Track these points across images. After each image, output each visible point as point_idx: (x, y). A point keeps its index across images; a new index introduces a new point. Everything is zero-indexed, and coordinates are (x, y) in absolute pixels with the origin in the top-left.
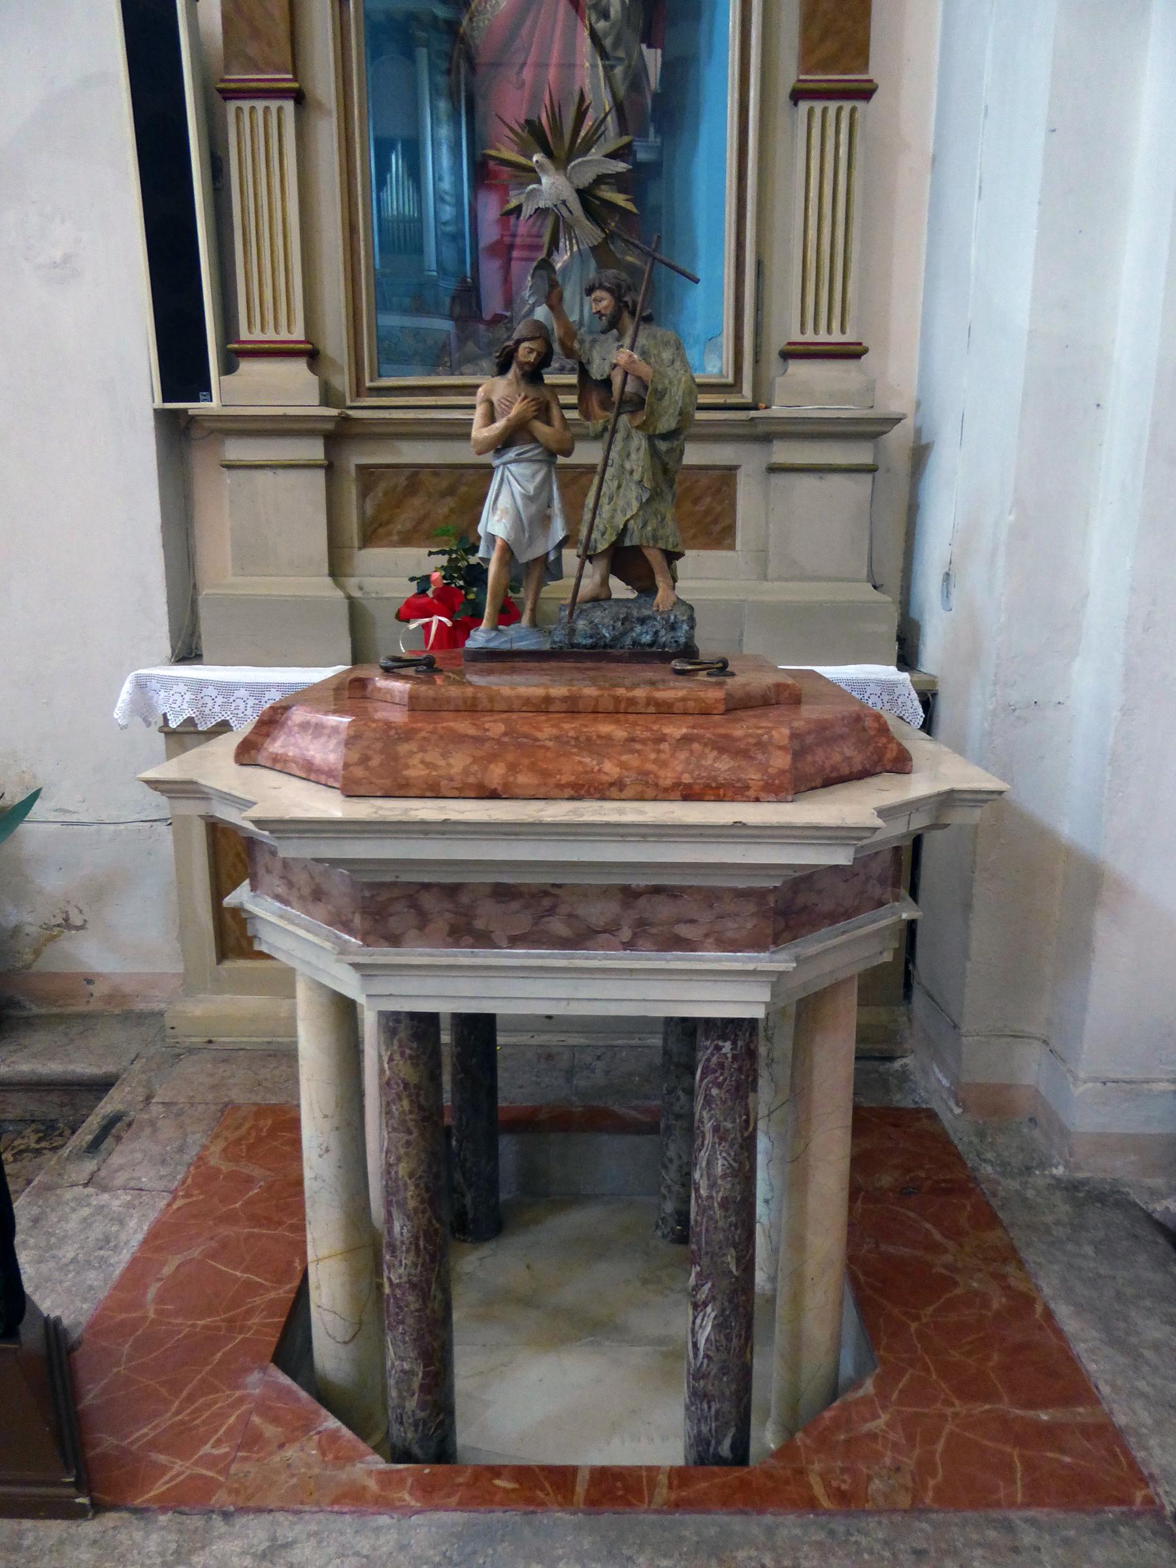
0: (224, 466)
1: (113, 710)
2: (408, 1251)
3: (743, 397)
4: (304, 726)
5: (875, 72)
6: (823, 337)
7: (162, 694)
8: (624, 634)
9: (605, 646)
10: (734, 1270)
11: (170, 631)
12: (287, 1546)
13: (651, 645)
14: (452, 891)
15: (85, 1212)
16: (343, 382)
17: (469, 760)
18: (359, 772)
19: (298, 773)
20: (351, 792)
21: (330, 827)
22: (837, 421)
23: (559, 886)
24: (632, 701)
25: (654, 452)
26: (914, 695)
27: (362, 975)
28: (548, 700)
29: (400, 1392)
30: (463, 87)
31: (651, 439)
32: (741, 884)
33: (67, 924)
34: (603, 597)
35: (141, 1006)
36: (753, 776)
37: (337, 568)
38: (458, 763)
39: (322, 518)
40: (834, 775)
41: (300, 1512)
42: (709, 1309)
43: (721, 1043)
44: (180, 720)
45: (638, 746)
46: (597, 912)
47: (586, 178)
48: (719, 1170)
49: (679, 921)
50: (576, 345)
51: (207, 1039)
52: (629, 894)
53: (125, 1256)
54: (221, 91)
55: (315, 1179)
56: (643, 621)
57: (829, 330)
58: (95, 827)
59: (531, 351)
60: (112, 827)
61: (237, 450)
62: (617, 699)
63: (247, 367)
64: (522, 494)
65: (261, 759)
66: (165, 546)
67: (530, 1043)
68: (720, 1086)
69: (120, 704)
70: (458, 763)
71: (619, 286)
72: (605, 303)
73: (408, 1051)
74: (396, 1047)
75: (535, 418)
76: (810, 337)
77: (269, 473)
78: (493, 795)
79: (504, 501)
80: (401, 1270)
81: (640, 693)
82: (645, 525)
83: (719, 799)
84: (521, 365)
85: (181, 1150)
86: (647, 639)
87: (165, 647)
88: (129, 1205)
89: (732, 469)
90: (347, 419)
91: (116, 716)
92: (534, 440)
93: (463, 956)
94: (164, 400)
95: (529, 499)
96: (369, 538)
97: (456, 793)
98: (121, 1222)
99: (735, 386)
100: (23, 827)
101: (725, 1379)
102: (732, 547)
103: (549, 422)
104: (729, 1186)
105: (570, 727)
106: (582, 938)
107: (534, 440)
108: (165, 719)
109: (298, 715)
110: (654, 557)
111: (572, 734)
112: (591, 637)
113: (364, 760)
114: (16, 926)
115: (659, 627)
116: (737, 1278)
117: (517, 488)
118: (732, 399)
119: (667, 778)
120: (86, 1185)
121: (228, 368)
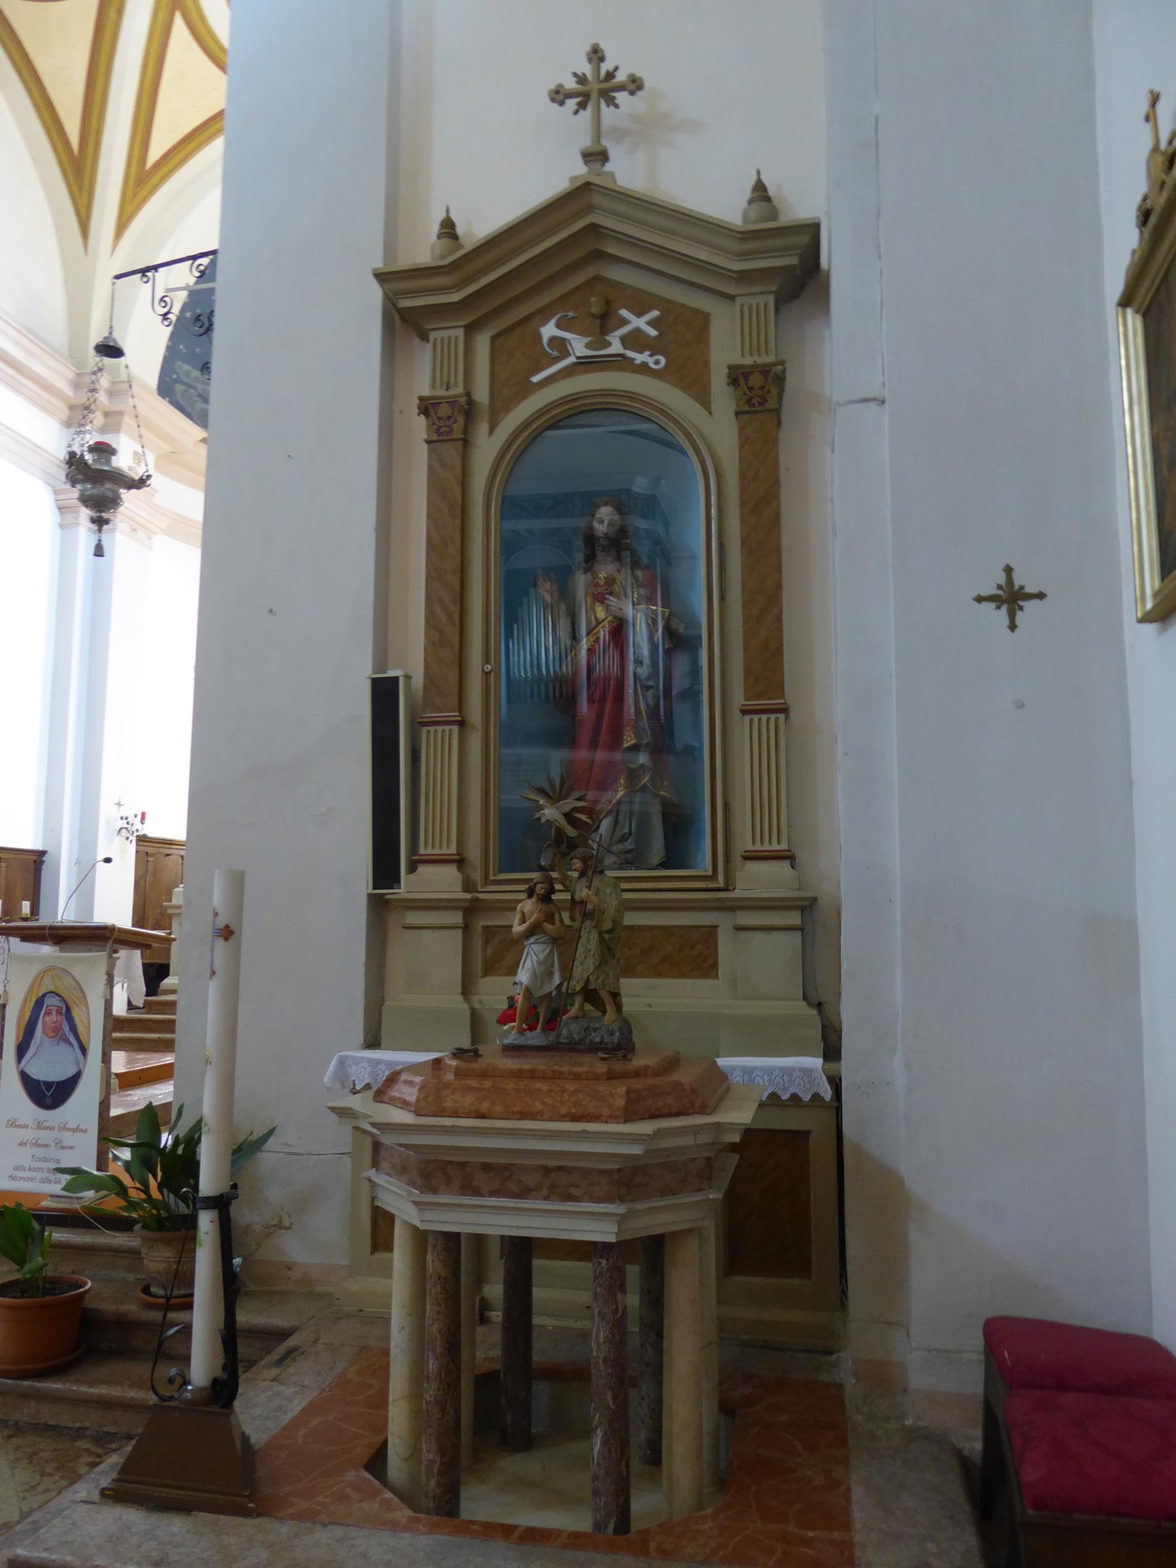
0: (404, 927)
1: (324, 1077)
2: (435, 1380)
3: (719, 883)
4: (405, 1082)
5: (792, 695)
6: (766, 847)
7: (354, 1068)
8: (586, 1037)
9: (576, 1044)
10: (611, 1403)
11: (365, 1028)
12: (352, 1538)
13: (601, 1043)
14: (463, 1165)
15: (270, 1393)
16: (477, 876)
17: (473, 1099)
18: (423, 1103)
19: (400, 1105)
20: (418, 1113)
21: (405, 1128)
22: (772, 899)
23: (513, 1165)
24: (561, 1073)
25: (601, 939)
26: (824, 1078)
27: (419, 1209)
28: (521, 1071)
29: (427, 1475)
30: (659, 578)
31: (600, 934)
32: (602, 1166)
33: (280, 1226)
34: (580, 1015)
35: (320, 1289)
36: (605, 1112)
37: (467, 990)
38: (468, 1100)
39: (459, 958)
40: (658, 1113)
41: (363, 1527)
42: (599, 1431)
43: (601, 1261)
44: (363, 1085)
45: (553, 1094)
46: (531, 1180)
47: (567, 809)
48: (601, 1339)
49: (572, 1185)
50: (568, 883)
51: (358, 1308)
52: (547, 1171)
53: (289, 1416)
54: (420, 723)
55: (396, 1346)
56: (595, 1030)
57: (770, 843)
58: (305, 1157)
59: (542, 888)
60: (316, 1157)
61: (412, 918)
62: (554, 1072)
63: (422, 869)
64: (537, 961)
65: (385, 1099)
66: (366, 975)
67: (575, 1326)
68: (601, 1286)
69: (328, 1073)
70: (468, 1100)
71: (584, 857)
72: (578, 865)
73: (441, 1257)
74: (435, 1254)
75: (545, 921)
76: (758, 847)
77: (430, 931)
78: (482, 1116)
79: (528, 964)
80: (431, 1393)
81: (565, 1069)
82: (597, 979)
83: (588, 1122)
84: (538, 895)
85: (331, 1369)
86: (598, 1040)
87: (360, 1038)
88: (296, 1393)
89: (715, 927)
90: (477, 899)
91: (325, 1081)
92: (544, 932)
93: (466, 1200)
94: (374, 888)
95: (540, 963)
96: (488, 970)
97: (465, 1115)
98: (290, 1401)
99: (714, 877)
100: (262, 1156)
101: (608, 1480)
102: (716, 977)
103: (553, 923)
104: (607, 1349)
105: (522, 1084)
106: (523, 1194)
107: (544, 932)
108: (354, 1085)
109: (404, 1077)
110: (604, 995)
111: (522, 1087)
112: (567, 1038)
113: (426, 1098)
114: (248, 1225)
115: (604, 1033)
116: (613, 1411)
117: (535, 958)
118: (711, 885)
119: (564, 1110)
120: (272, 1381)
121: (412, 869)
